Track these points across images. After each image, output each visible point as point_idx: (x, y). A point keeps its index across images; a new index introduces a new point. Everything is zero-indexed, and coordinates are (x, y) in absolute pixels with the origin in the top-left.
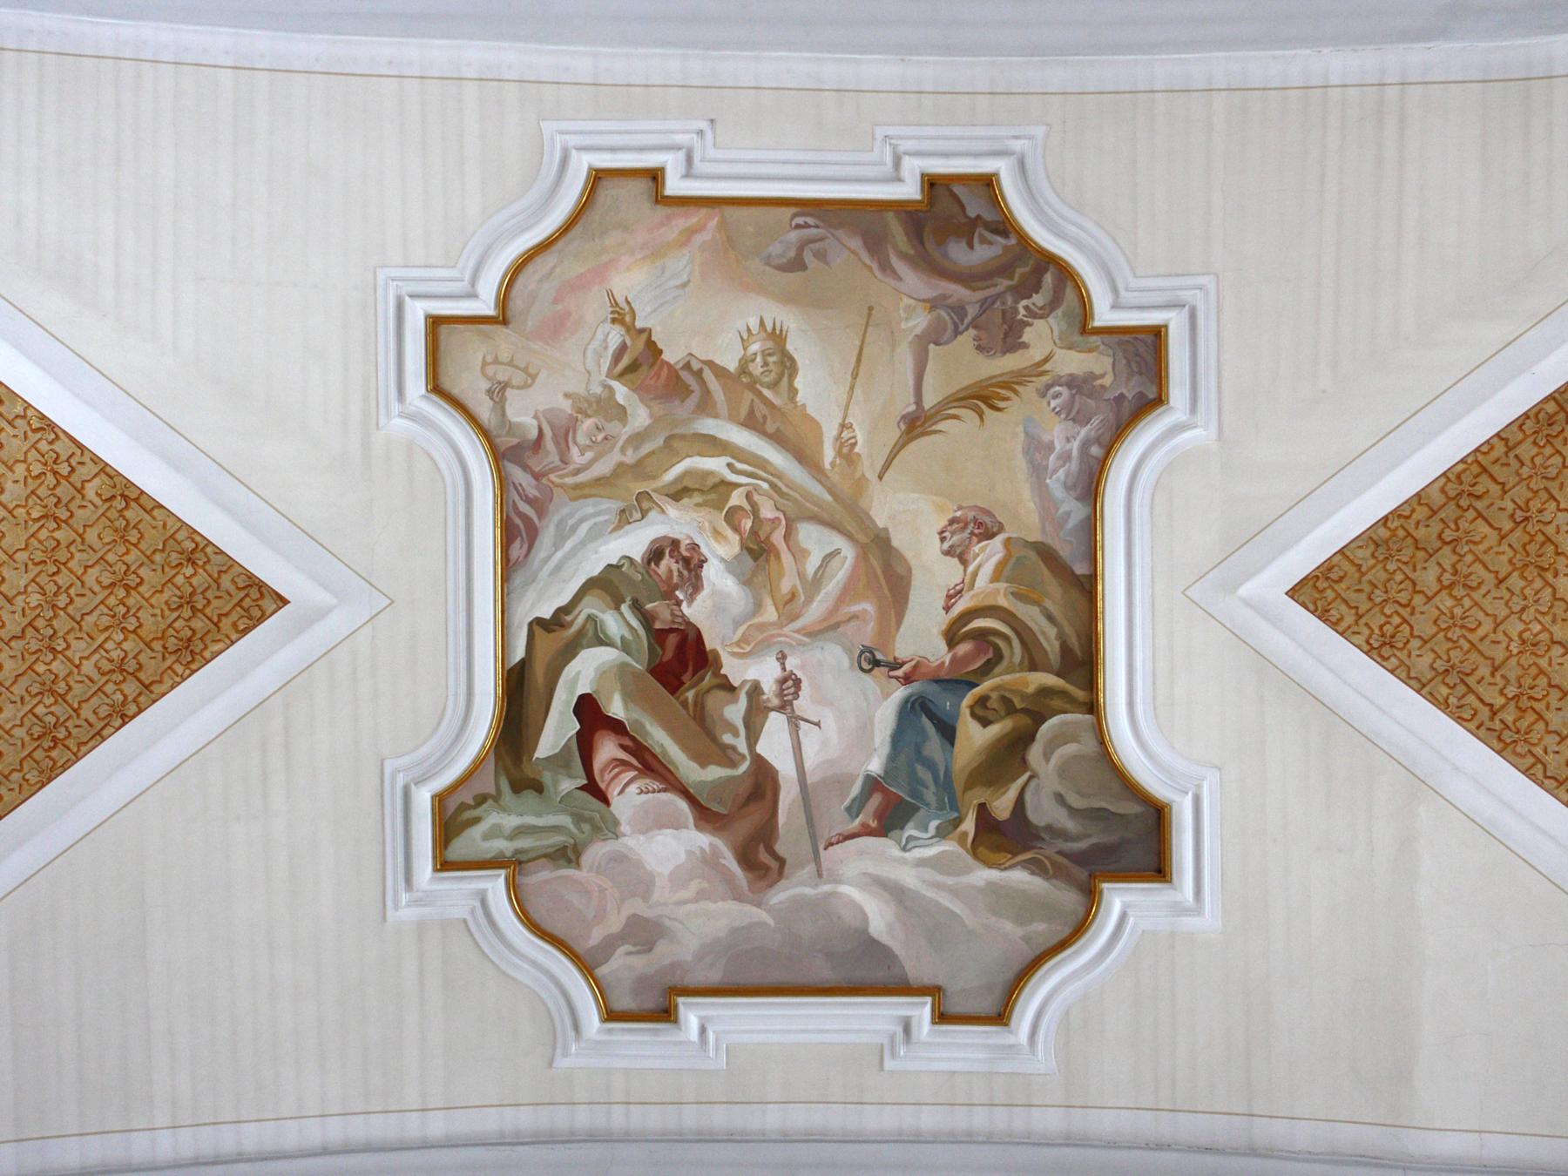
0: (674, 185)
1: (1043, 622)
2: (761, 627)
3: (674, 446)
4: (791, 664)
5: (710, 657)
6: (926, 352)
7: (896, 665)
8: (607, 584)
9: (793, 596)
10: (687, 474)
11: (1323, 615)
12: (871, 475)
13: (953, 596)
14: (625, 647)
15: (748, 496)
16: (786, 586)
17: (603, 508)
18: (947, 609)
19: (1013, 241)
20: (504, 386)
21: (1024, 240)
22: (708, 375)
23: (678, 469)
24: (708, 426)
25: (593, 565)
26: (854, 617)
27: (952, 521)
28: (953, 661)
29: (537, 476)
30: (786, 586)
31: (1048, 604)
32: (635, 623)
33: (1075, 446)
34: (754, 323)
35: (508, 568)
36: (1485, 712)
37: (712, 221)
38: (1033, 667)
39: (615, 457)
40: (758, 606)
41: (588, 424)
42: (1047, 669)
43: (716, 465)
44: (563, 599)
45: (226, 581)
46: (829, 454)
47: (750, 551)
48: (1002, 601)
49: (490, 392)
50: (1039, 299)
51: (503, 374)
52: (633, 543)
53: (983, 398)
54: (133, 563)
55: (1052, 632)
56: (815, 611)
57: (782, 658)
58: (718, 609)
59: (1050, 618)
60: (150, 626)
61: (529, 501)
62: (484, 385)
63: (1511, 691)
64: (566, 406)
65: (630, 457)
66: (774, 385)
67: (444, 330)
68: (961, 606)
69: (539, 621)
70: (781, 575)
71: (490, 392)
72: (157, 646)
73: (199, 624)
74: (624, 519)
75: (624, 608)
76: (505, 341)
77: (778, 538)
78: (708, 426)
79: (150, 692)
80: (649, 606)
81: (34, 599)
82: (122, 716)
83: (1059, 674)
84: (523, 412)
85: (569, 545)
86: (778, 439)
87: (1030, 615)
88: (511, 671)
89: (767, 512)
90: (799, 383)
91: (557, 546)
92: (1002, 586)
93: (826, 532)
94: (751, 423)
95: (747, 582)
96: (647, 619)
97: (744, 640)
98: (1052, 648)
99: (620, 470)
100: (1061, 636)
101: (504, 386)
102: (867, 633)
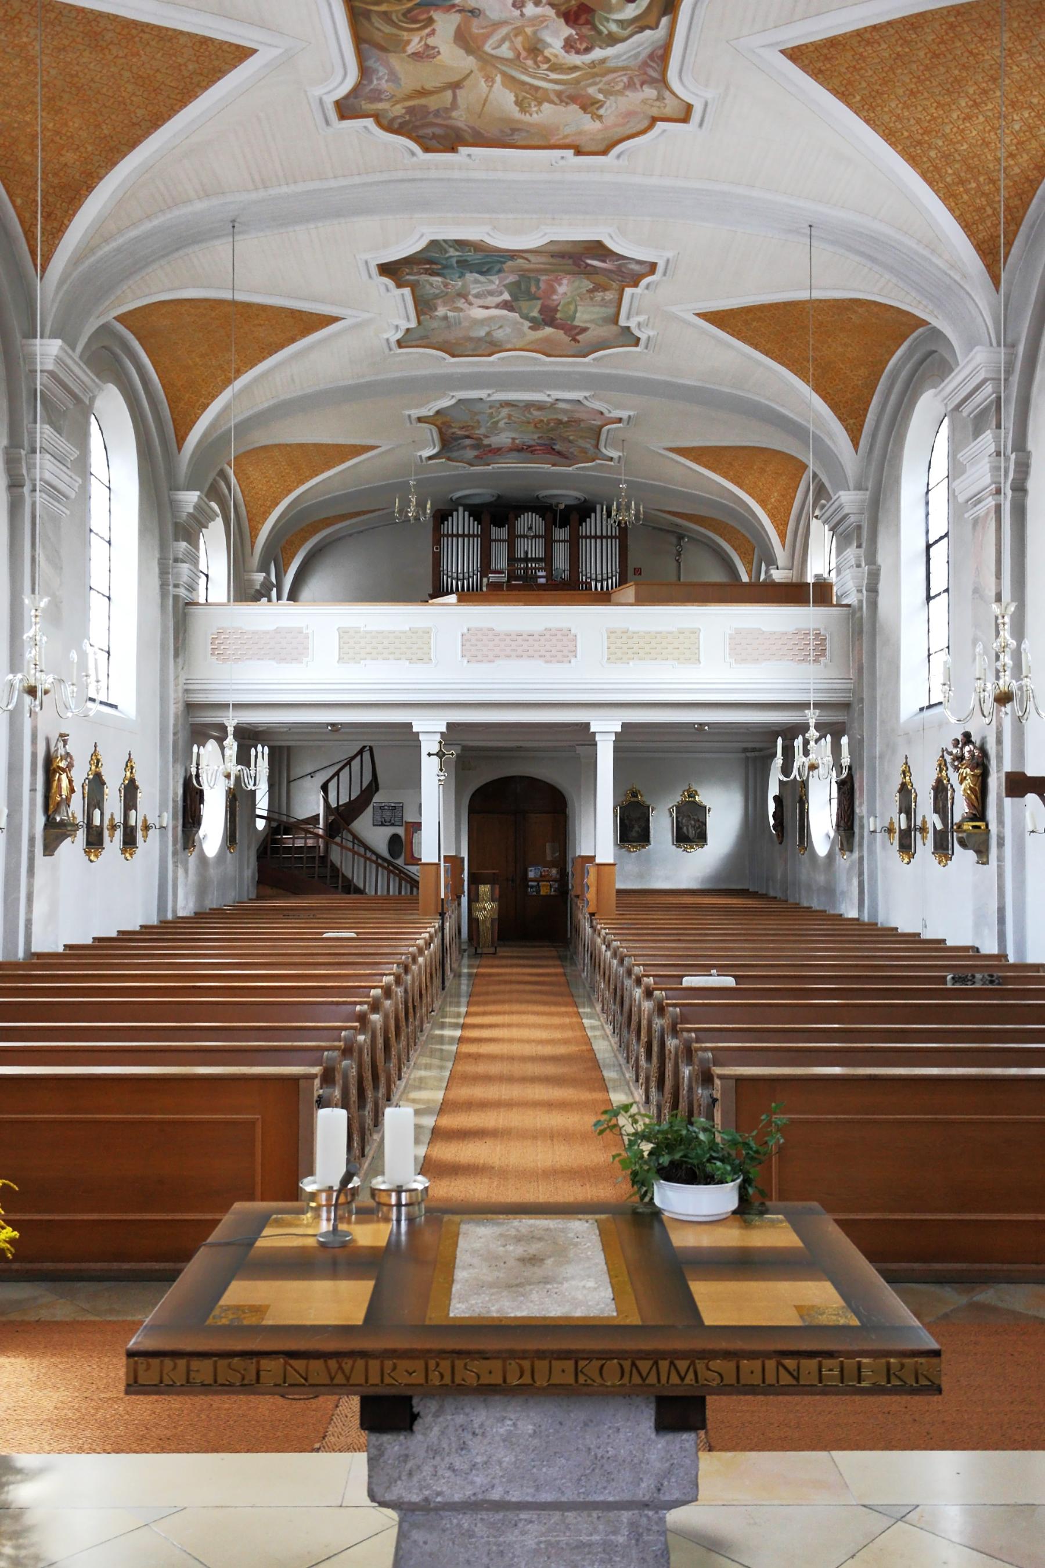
0: (572, 151)
1: (382, 28)
2: (534, 25)
3: (577, 81)
4: (519, 12)
5: (452, 753)
6: (418, 1358)
7: (460, 11)
8: (613, 40)
9: (516, 36)
10: (568, 74)
11: (238, 46)
12: (476, 71)
13: (433, 32)
14: (607, 20)
15: (539, 67)
16: (520, 39)
17: (611, 64)
18: (434, 30)
19: (414, 134)
20: (657, 99)
21: (410, 137)
22: (558, 102)
23: (573, 75)
24: (557, 87)
25: (619, 48)
26: (483, 28)
27: (434, 57)
28: (429, 12)
29: (645, 73)
30: (520, 39)
31: (380, 34)
32: (601, 27)
33: (375, 82)
34: (535, 115)
35: (667, 47)
36: (147, 30)
37: (553, 141)
38: (385, 13)
39: (605, 79)
40: (535, 33)
41: (617, 88)
42: (376, 12)
43: (553, 76)
44: (637, 38)
45: (806, 62)
46: (498, 78)
47: (538, 50)
48: (405, 33)
49: (664, 99)
50: (399, 121)
51: (658, 103)
52: (597, 54)
53: (422, 93)
54: (458, 848)
55: (377, 25)
56: (504, 31)
57: (522, 15)
58: (556, 33)
59: (379, 29)
60: (849, 55)
61: (651, 67)
62: (666, 101)
63: (137, 39)
64: (627, 93)
65: (598, 79)
66: (525, 98)
67: (682, 116)
68: (427, 31)
69: (652, 28)
70: (523, 43)
71: (664, 99)
72: (848, 47)
73: (826, 51)
74: (603, 61)
75: (606, 32)
76: (655, 112)
77: (524, 54)
78: (557, 87)
79: (858, 33)
80: (593, 33)
81: (899, 71)
82: (875, 28)
83: (370, 11)
84: (650, 92)
85: (633, 53)
86: (524, 83)
87: (388, 29)
88: (670, 13)
89: (530, 63)
90: (514, 99)
91: (639, 53)
92: (406, 38)
93: (501, 55)
94: (537, 88)
95: (540, 40)
96: (595, 28)
97: (542, 22)
98: (377, 22)
99: (603, 75)
100: (372, 24)
101: (657, 99)
102: (475, 22)
